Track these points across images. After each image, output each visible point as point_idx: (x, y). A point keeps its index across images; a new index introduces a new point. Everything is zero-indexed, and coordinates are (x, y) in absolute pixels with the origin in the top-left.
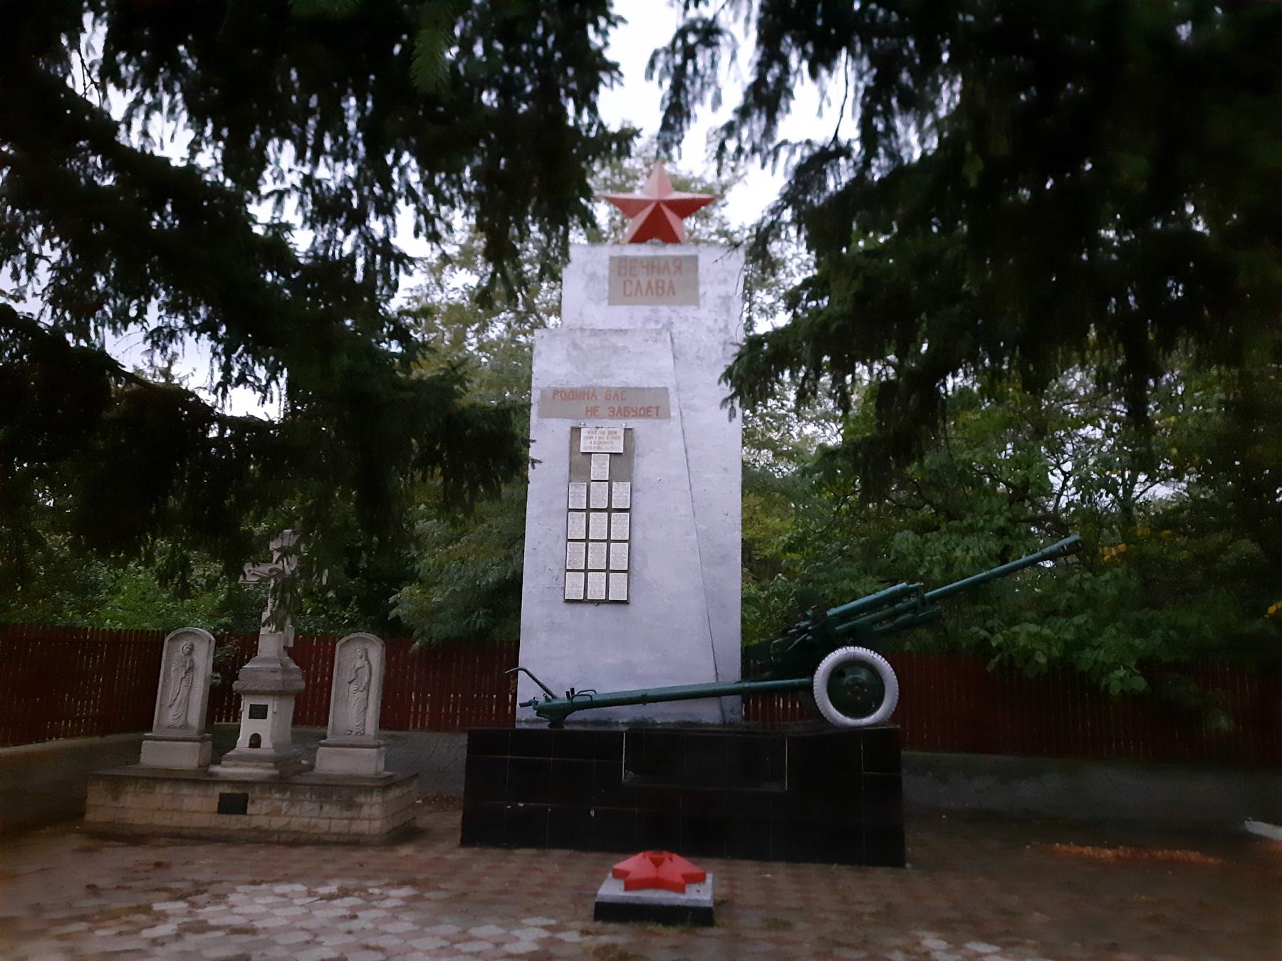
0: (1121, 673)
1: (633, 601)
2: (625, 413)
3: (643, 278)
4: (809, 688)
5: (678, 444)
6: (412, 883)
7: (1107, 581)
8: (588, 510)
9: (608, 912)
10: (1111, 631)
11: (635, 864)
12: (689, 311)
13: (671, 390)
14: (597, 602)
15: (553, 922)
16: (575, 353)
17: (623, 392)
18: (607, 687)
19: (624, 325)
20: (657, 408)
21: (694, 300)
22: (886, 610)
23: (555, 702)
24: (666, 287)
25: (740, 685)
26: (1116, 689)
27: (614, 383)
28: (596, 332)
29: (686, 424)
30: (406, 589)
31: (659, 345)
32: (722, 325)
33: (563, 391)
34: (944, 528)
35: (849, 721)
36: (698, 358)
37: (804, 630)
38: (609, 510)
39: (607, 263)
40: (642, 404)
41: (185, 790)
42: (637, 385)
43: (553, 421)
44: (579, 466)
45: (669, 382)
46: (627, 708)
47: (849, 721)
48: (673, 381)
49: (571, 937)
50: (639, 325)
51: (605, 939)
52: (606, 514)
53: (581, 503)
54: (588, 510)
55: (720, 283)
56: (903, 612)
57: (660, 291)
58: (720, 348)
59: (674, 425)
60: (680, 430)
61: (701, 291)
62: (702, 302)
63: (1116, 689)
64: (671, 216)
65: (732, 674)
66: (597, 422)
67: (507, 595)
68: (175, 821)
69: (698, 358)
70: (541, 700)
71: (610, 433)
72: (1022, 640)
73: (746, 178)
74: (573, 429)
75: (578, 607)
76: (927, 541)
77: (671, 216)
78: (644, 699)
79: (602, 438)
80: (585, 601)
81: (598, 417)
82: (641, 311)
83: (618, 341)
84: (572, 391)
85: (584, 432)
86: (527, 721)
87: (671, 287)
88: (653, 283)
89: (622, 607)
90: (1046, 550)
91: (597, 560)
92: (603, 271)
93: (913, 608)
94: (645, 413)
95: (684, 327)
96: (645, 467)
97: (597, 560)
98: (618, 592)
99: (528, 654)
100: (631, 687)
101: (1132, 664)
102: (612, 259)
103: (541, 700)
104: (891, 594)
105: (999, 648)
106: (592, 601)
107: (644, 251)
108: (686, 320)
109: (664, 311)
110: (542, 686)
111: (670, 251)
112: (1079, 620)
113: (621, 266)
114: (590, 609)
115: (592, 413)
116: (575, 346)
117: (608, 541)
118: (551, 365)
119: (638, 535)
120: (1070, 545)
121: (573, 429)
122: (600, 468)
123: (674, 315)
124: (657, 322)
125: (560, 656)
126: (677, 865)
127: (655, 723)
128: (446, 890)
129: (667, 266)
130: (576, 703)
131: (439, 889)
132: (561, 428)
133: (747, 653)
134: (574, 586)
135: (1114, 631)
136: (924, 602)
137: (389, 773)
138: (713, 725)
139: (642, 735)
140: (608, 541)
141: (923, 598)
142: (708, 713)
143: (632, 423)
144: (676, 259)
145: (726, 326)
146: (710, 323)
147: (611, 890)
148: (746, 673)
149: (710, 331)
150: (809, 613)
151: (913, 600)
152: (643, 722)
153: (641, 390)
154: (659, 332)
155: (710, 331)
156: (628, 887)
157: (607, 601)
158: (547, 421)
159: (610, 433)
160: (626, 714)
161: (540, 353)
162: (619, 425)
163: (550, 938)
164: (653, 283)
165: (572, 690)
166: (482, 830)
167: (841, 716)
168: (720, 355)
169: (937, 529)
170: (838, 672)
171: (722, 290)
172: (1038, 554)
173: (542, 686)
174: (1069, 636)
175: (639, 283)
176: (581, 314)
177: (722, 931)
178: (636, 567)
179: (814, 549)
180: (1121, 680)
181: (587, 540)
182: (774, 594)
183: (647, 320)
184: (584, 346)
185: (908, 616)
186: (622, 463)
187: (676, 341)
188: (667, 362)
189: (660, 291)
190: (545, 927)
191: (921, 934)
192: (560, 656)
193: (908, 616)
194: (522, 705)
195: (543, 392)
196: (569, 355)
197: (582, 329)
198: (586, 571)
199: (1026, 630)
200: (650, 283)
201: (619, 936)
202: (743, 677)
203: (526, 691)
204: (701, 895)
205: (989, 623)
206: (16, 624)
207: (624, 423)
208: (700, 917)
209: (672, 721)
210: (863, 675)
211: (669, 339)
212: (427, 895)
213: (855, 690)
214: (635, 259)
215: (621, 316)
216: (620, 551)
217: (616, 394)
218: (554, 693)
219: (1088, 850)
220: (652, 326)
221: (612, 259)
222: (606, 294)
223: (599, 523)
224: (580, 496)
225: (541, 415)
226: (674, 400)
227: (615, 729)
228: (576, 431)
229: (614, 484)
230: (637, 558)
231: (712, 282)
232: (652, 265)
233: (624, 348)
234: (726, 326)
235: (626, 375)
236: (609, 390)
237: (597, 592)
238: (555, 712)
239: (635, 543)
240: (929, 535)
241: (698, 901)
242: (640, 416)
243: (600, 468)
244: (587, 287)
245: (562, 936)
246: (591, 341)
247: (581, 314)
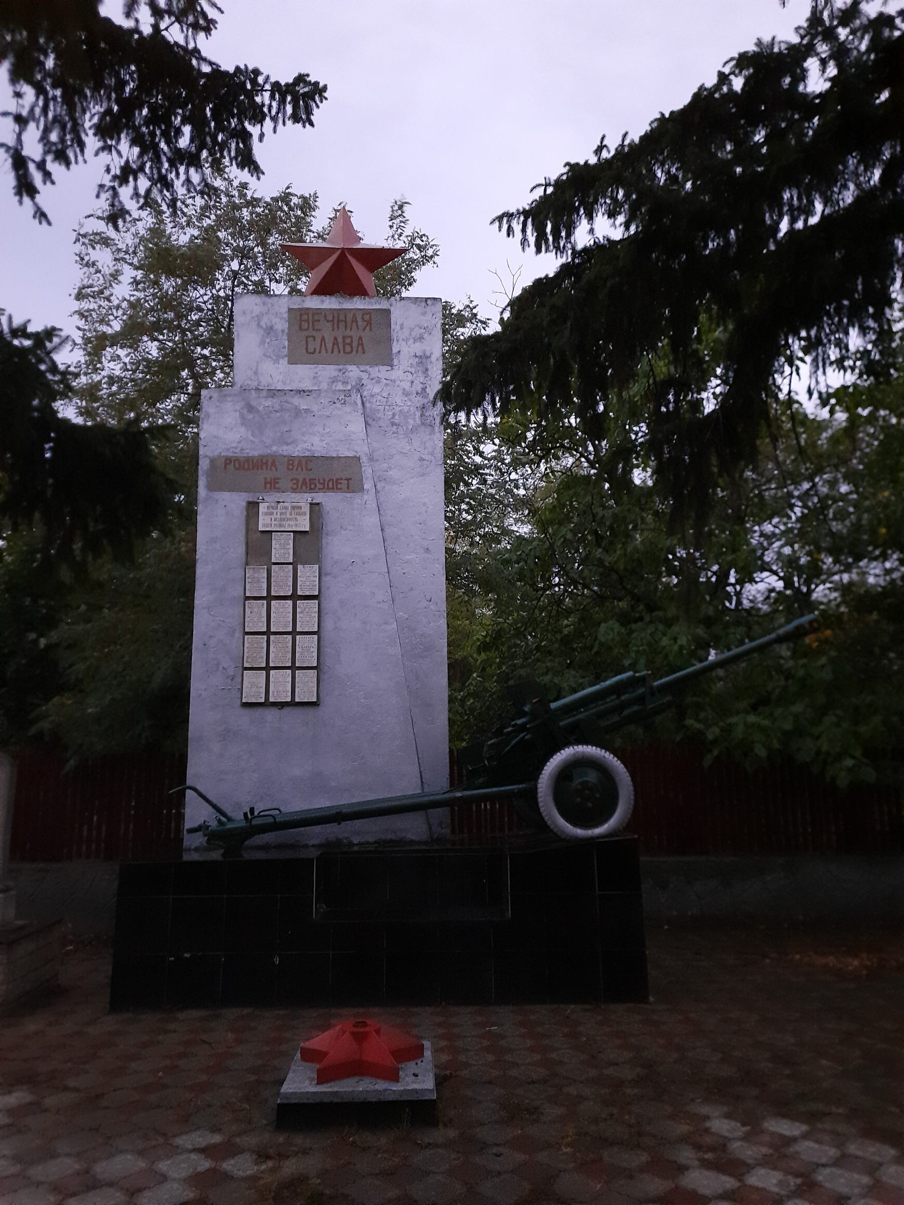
0: (849, 762)
1: (326, 700)
2: (310, 486)
3: (328, 332)
4: (533, 793)
5: (371, 520)
6: (27, 1079)
7: (823, 666)
8: (269, 598)
9: (297, 1116)
10: (829, 719)
11: (330, 1037)
12: (381, 371)
13: (364, 459)
14: (281, 705)
15: (217, 1139)
16: (250, 416)
17: (308, 461)
18: (296, 804)
19: (307, 385)
20: (348, 480)
21: (387, 359)
22: (611, 701)
23: (230, 826)
24: (355, 344)
25: (447, 796)
26: (843, 781)
27: (296, 451)
28: (273, 393)
29: (381, 499)
30: (56, 700)
31: (347, 409)
32: (419, 388)
33: (237, 459)
34: (647, 618)
35: (580, 832)
36: (393, 424)
37: (522, 728)
38: (294, 597)
39: (286, 316)
40: (334, 475)
42: (324, 453)
43: (226, 495)
44: (257, 546)
45: (362, 450)
46: (317, 829)
47: (580, 832)
48: (366, 449)
49: (241, 1166)
50: (324, 386)
51: (290, 1167)
52: (290, 602)
53: (260, 589)
54: (269, 598)
55: (415, 341)
56: (629, 703)
57: (348, 349)
58: (418, 414)
59: (369, 497)
60: (375, 505)
61: (395, 350)
62: (396, 362)
63: (843, 781)
64: (360, 270)
65: (439, 781)
66: (277, 496)
67: (173, 701)
69: (393, 424)
70: (213, 824)
71: (293, 508)
72: (739, 732)
73: (436, 259)
74: (249, 503)
75: (259, 711)
76: (632, 631)
77: (360, 270)
78: (338, 816)
80: (267, 704)
81: (278, 490)
82: (328, 371)
83: (303, 403)
84: (248, 460)
85: (263, 508)
86: (196, 849)
87: (361, 343)
88: (340, 340)
89: (310, 711)
90: (781, 631)
91: (280, 652)
92: (281, 325)
93: (641, 700)
94: (334, 485)
95: (377, 390)
96: (337, 547)
97: (280, 652)
98: (307, 690)
99: (202, 767)
100: (322, 803)
101: (858, 753)
102: (290, 310)
103: (213, 824)
104: (617, 683)
105: (715, 741)
106: (275, 704)
107: (329, 303)
108: (378, 382)
109: (354, 371)
110: (214, 806)
111: (358, 304)
112: (798, 708)
113: (302, 319)
114: (271, 715)
115: (272, 485)
116: (251, 408)
117: (294, 633)
118: (221, 430)
119: (328, 624)
120: (811, 622)
121: (249, 503)
122: (282, 549)
123: (364, 376)
124: (345, 383)
125: (232, 768)
126: (385, 1028)
127: (351, 844)
128: (77, 1090)
129: (354, 320)
130: (257, 825)
131: (66, 1089)
132: (235, 502)
133: (457, 759)
134: (253, 687)
135: (834, 719)
136: (653, 692)
137: (20, 923)
138: (420, 843)
139: (335, 856)
140: (294, 633)
141: (651, 688)
142: (413, 828)
143: (319, 497)
144: (365, 312)
145: (424, 389)
146: (407, 385)
147: (300, 1082)
148: (455, 780)
149: (406, 394)
150: (526, 709)
151: (641, 690)
152: (338, 843)
153: (328, 460)
154: (348, 393)
155: (406, 394)
156: (322, 1078)
157: (293, 704)
158: (217, 495)
159: (293, 508)
160: (316, 834)
161: (208, 416)
162: (304, 500)
163: (213, 1171)
164: (340, 340)
165: (252, 810)
166: (141, 986)
167: (561, 822)
168: (418, 421)
169: (641, 619)
170: (565, 773)
171: (418, 348)
172: (773, 636)
173: (214, 806)
174: (788, 726)
175: (323, 339)
176: (256, 373)
177: (452, 1133)
178: (327, 661)
179: (510, 648)
180: (850, 770)
181: (268, 633)
182: (470, 695)
183: (334, 380)
184: (261, 408)
185: (635, 708)
186: (309, 544)
187: (368, 405)
188: (357, 426)
189: (348, 349)
190: (205, 1151)
191: (705, 1110)
192: (232, 768)
193: (635, 708)
194: (191, 831)
195: (213, 461)
196: (242, 417)
197: (257, 389)
198: (268, 669)
199: (742, 722)
200: (336, 339)
201: (309, 1159)
202: (452, 784)
203: (195, 813)
204: (419, 1080)
205: (702, 715)
207: (308, 497)
208: (418, 1112)
209: (371, 840)
210: (592, 777)
211: (359, 401)
212: (49, 1102)
213: (585, 795)
214: (318, 311)
215: (304, 375)
216: (307, 649)
217: (300, 464)
218: (229, 814)
219: (831, 960)
220: (340, 386)
221: (290, 310)
222: (286, 351)
223: (282, 612)
224: (258, 581)
225: (211, 488)
226: (367, 471)
227: (303, 854)
228: (252, 507)
229: (300, 567)
230: (327, 650)
231: (406, 340)
232: (337, 318)
233: (307, 411)
234: (424, 389)
235: (314, 441)
236: (291, 459)
237: (281, 690)
238: (230, 836)
239: (325, 634)
240: (634, 626)
241: (416, 1091)
242: (329, 489)
243: (282, 549)
244: (263, 342)
245: (228, 1165)
246: (269, 403)
247: (256, 373)
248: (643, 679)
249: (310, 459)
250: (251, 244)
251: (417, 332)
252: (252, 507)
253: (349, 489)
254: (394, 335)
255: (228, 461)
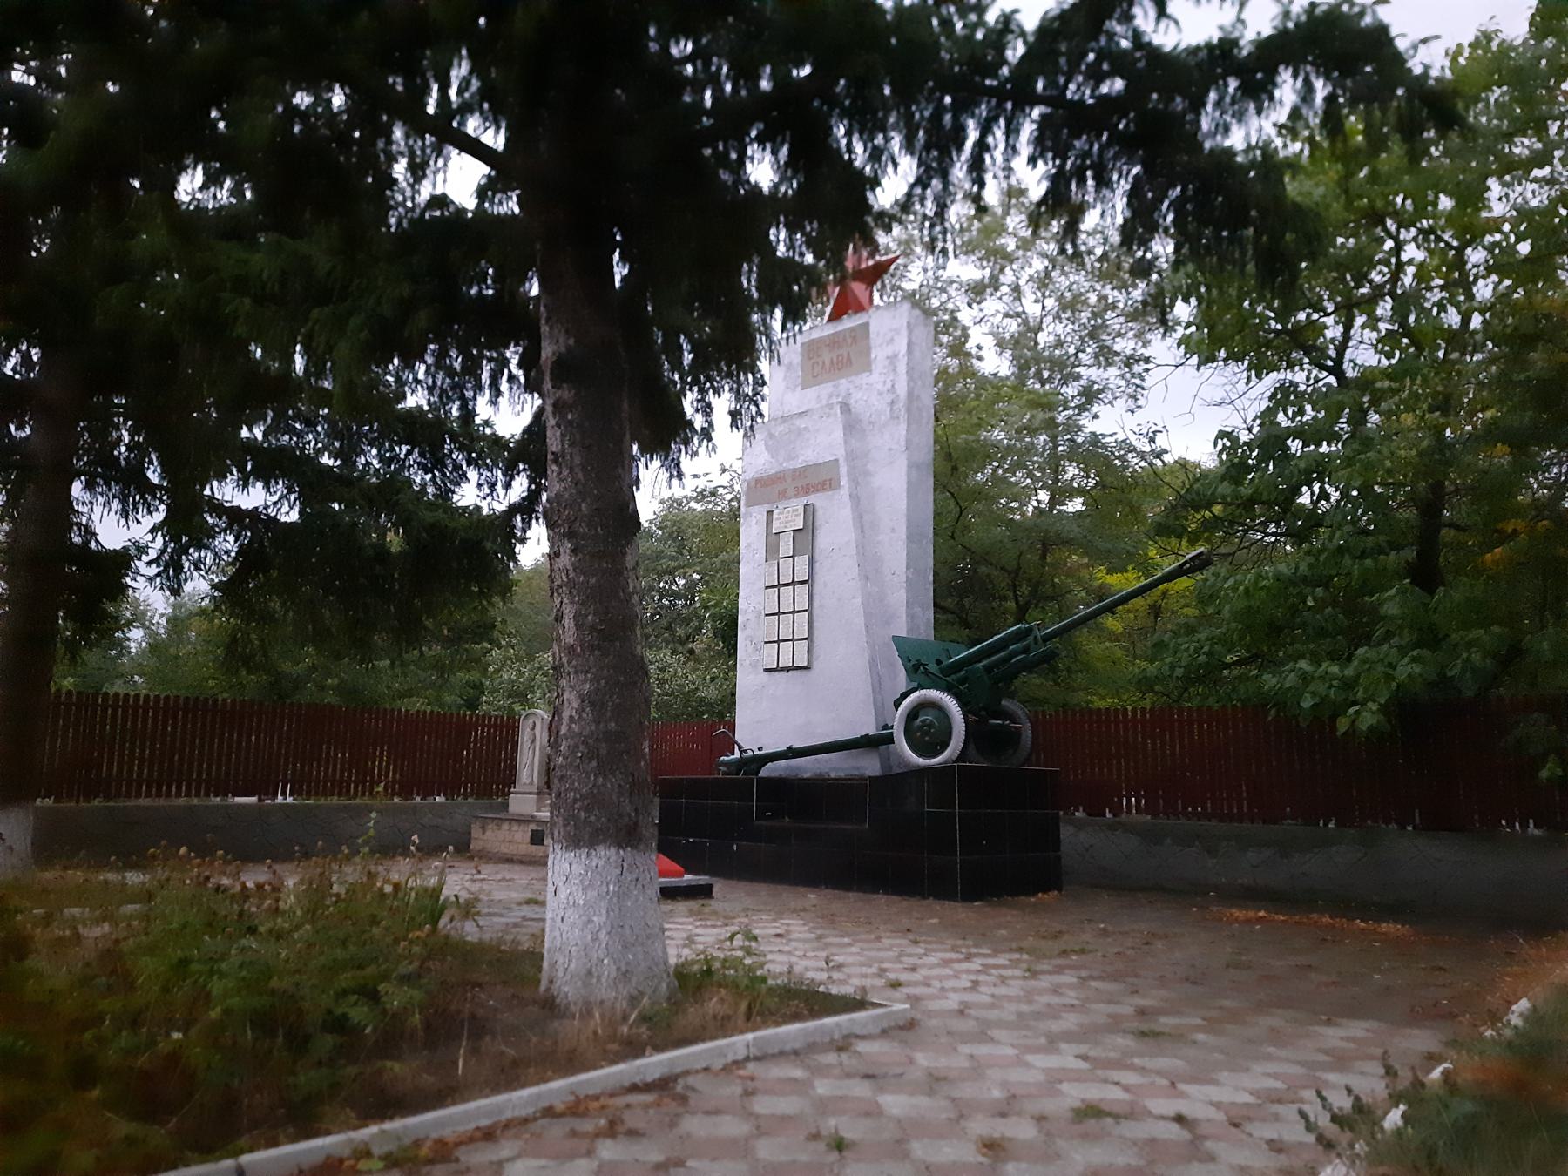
1: (816, 665)
2: (806, 490)
3: (827, 356)
12: (863, 379)
14: (788, 670)
27: (798, 464)
32: (889, 385)
35: (921, 761)
41: (515, 827)
44: (772, 540)
47: (921, 761)
59: (844, 492)
68: (505, 849)
78: (792, 753)
79: (789, 517)
81: (787, 498)
83: (801, 423)
85: (775, 515)
89: (804, 672)
93: (1026, 650)
96: (823, 540)
106: (783, 669)
115: (783, 495)
122: (786, 546)
143: (812, 499)
144: (852, 330)
146: (880, 386)
155: (880, 394)
162: (798, 504)
167: (909, 751)
171: (889, 351)
206: (117, 694)
209: (842, 775)
228: (770, 513)
236: (794, 470)
239: (816, 611)
246: (781, 428)
248: (1030, 630)
249: (806, 468)
250: (1140, 254)
251: (888, 338)
252: (770, 513)
253: (831, 489)
254: (872, 343)
255: (757, 481)
